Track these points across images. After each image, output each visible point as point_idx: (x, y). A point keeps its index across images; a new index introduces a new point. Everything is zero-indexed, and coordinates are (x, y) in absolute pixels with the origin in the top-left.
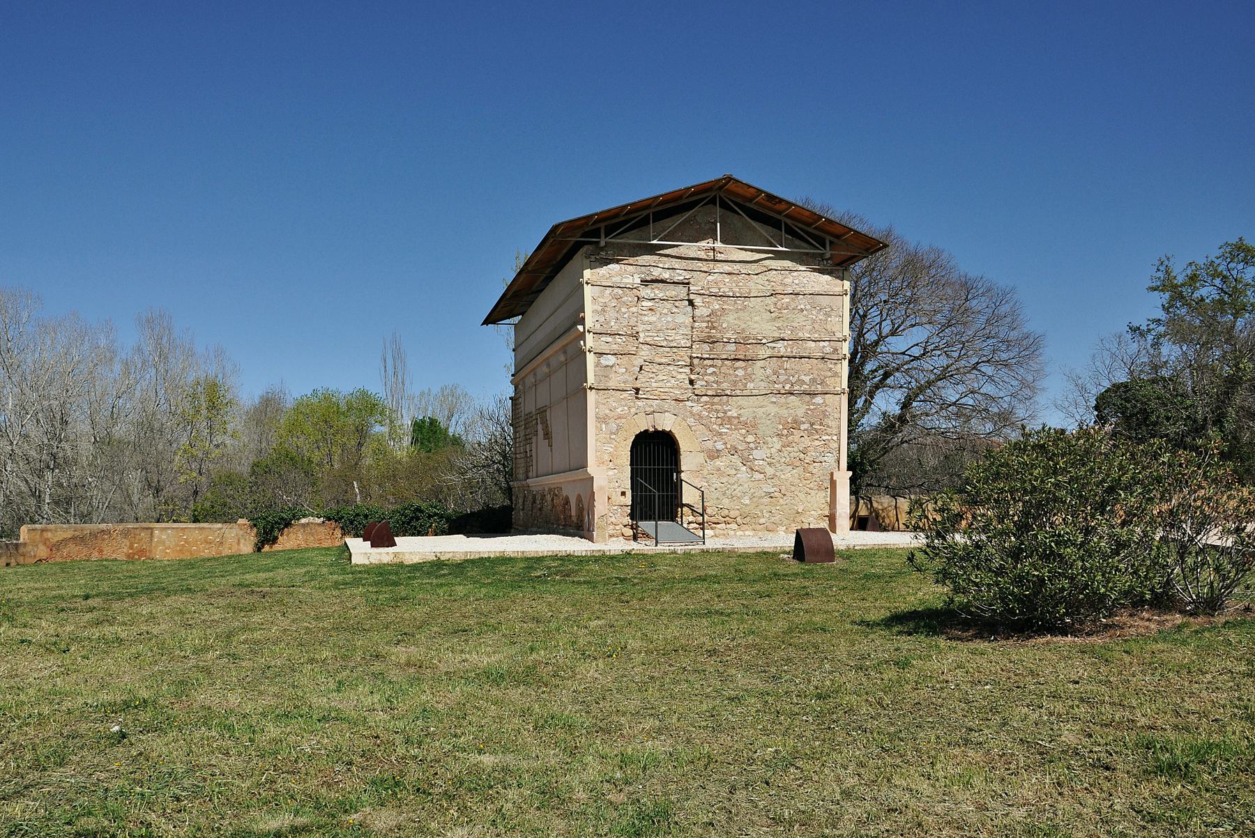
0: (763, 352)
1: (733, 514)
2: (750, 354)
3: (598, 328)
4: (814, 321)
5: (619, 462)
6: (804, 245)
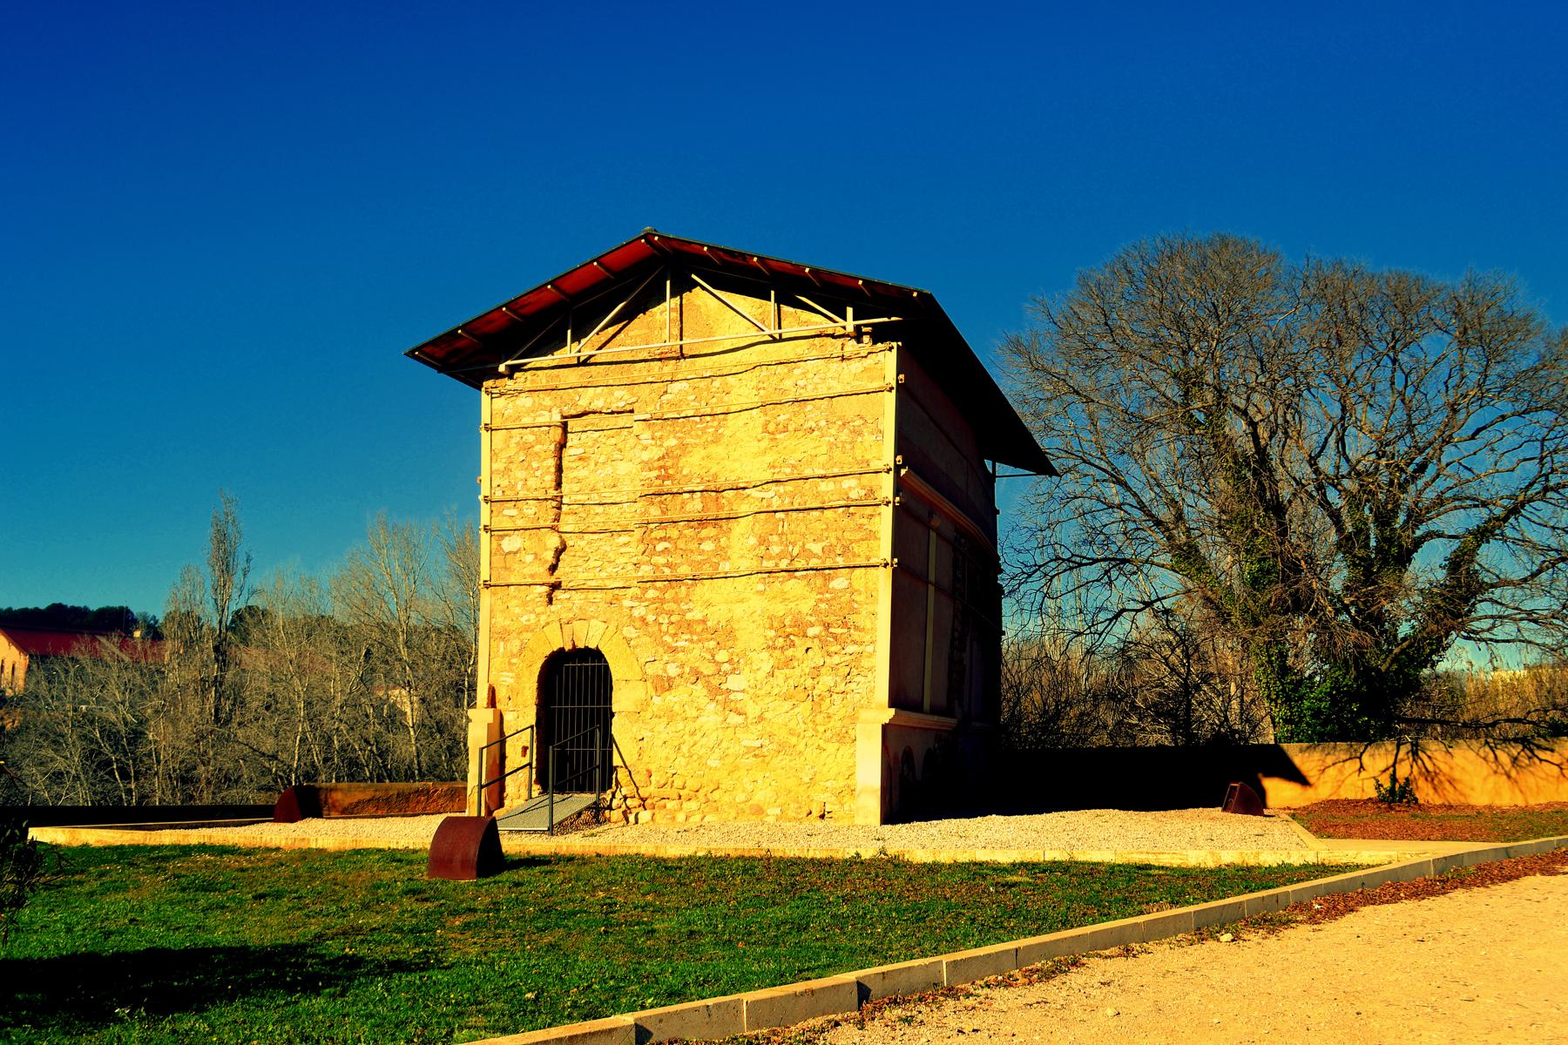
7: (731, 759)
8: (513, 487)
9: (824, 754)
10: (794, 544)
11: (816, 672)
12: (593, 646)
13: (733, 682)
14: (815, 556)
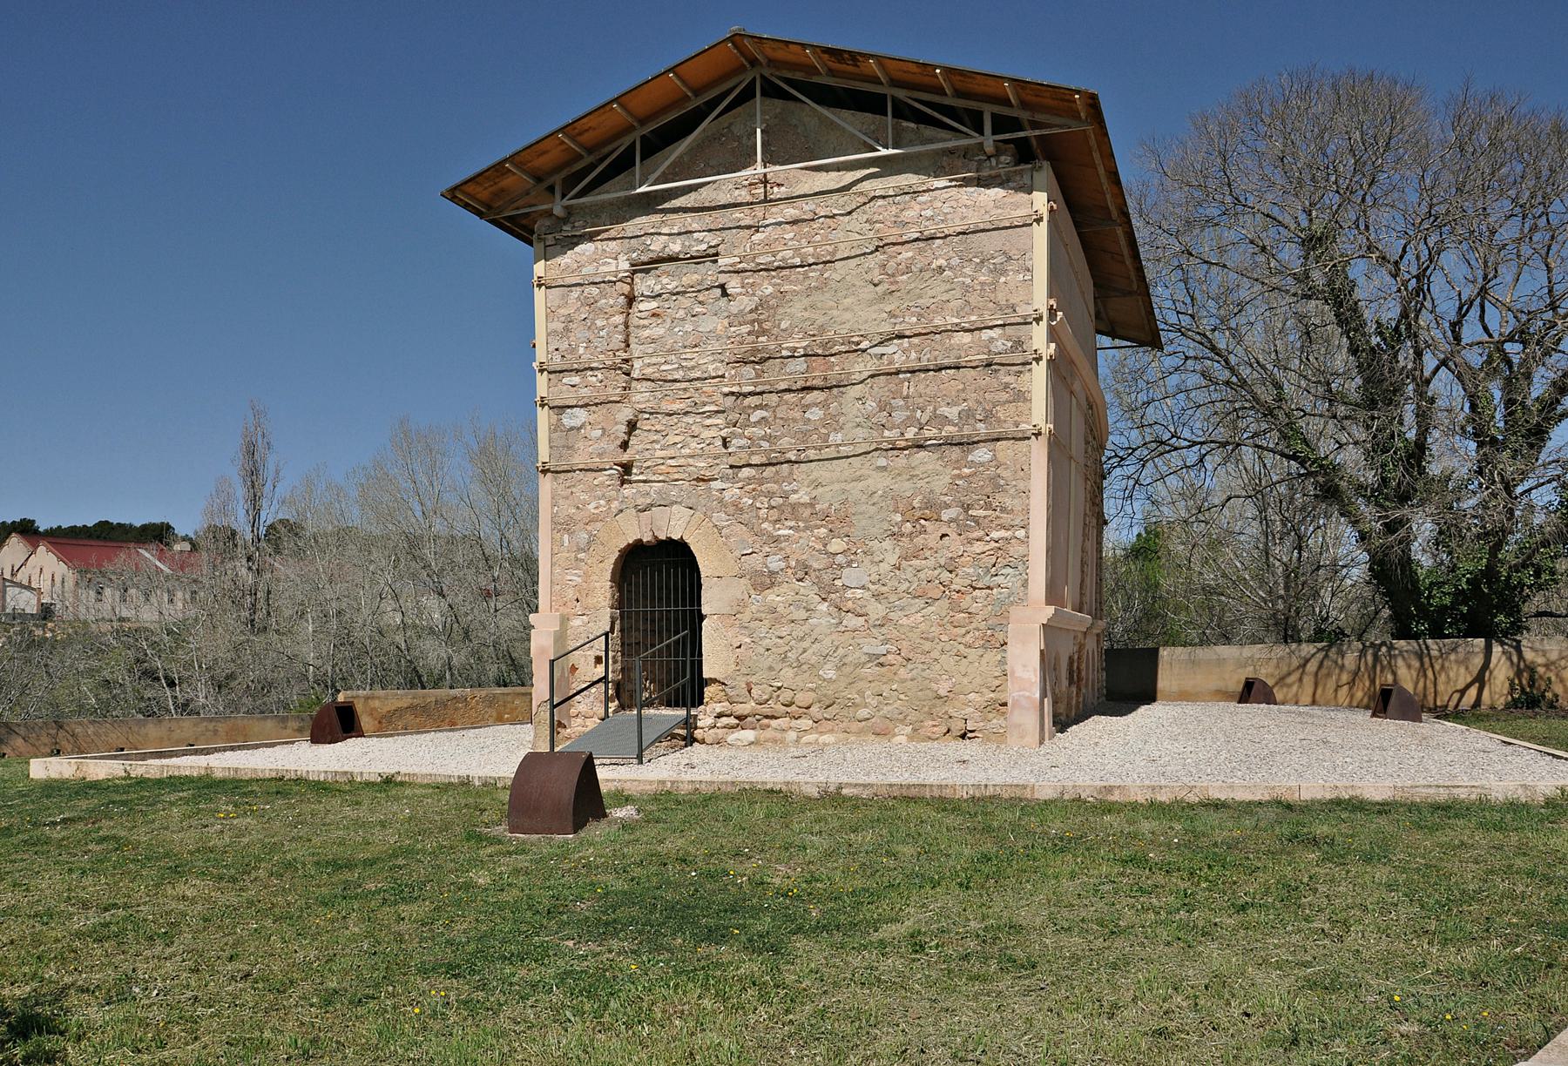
0: (861, 367)
1: (802, 698)
2: (834, 375)
3: (557, 362)
4: (967, 289)
5: (591, 601)
6: (943, 134)
8: (573, 350)
12: (676, 537)
14: (950, 422)
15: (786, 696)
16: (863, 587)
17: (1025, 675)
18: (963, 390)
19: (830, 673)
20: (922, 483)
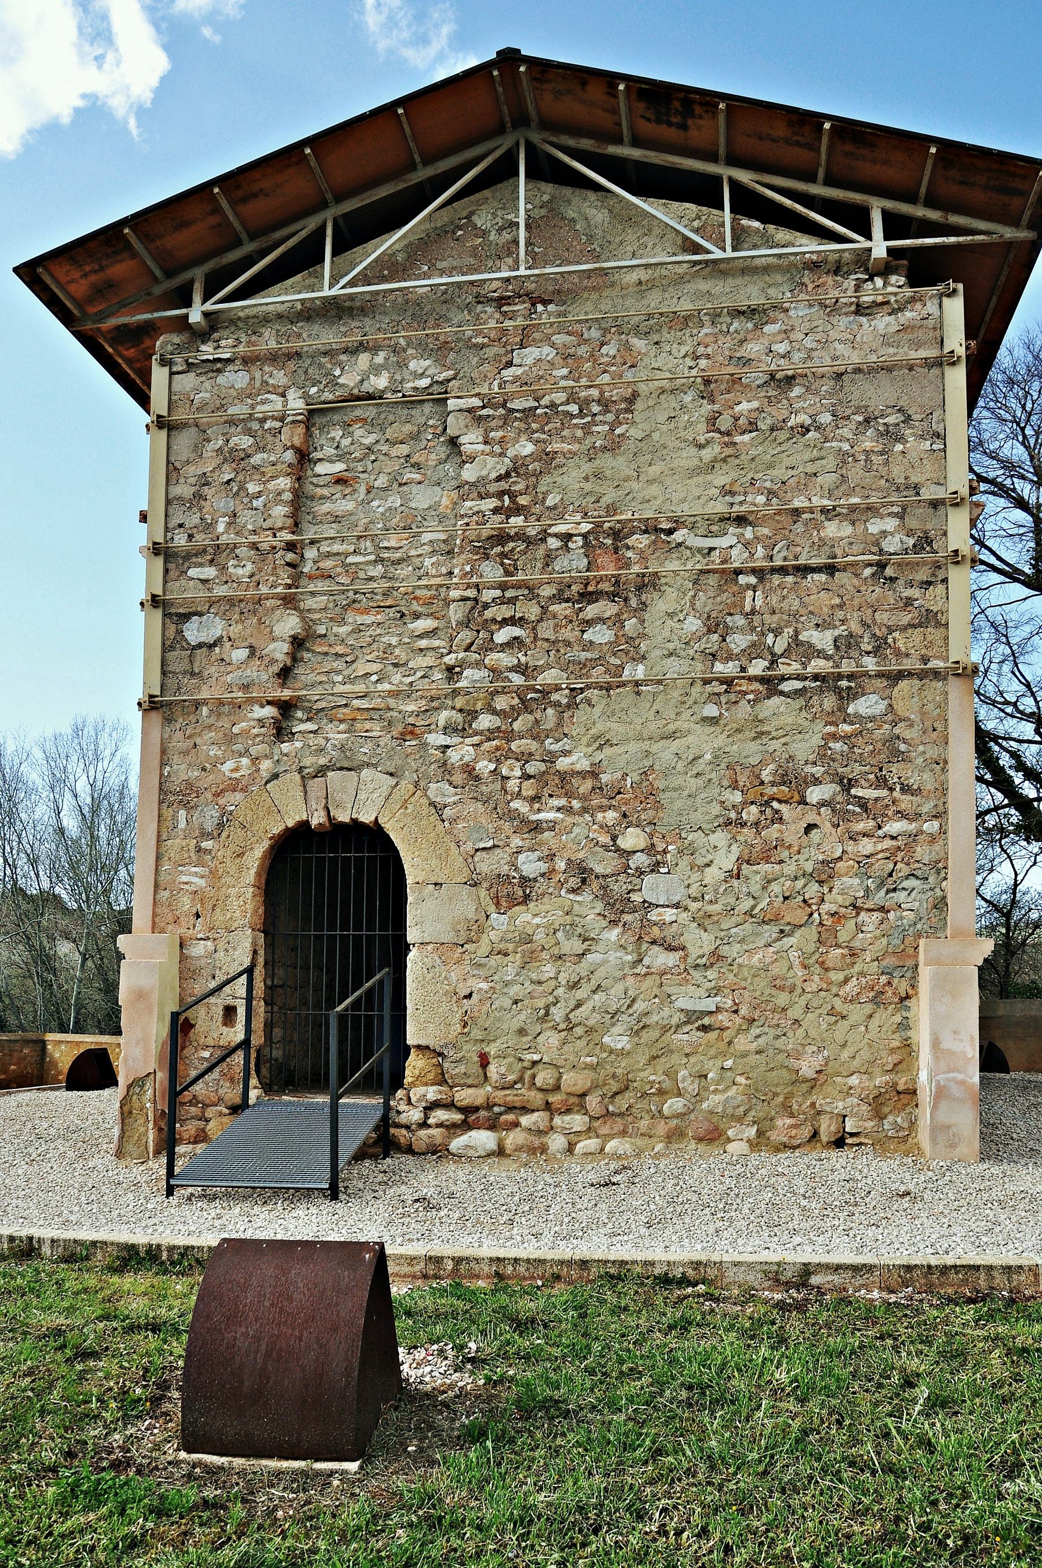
1: (572, 1081)
7: (654, 1034)
8: (209, 527)
9: (844, 1025)
10: (777, 632)
11: (825, 874)
12: (366, 817)
13: (654, 888)
14: (820, 654)
15: (544, 1077)
16: (677, 906)
17: (957, 1047)
18: (841, 606)
19: (617, 1039)
20: (776, 744)
